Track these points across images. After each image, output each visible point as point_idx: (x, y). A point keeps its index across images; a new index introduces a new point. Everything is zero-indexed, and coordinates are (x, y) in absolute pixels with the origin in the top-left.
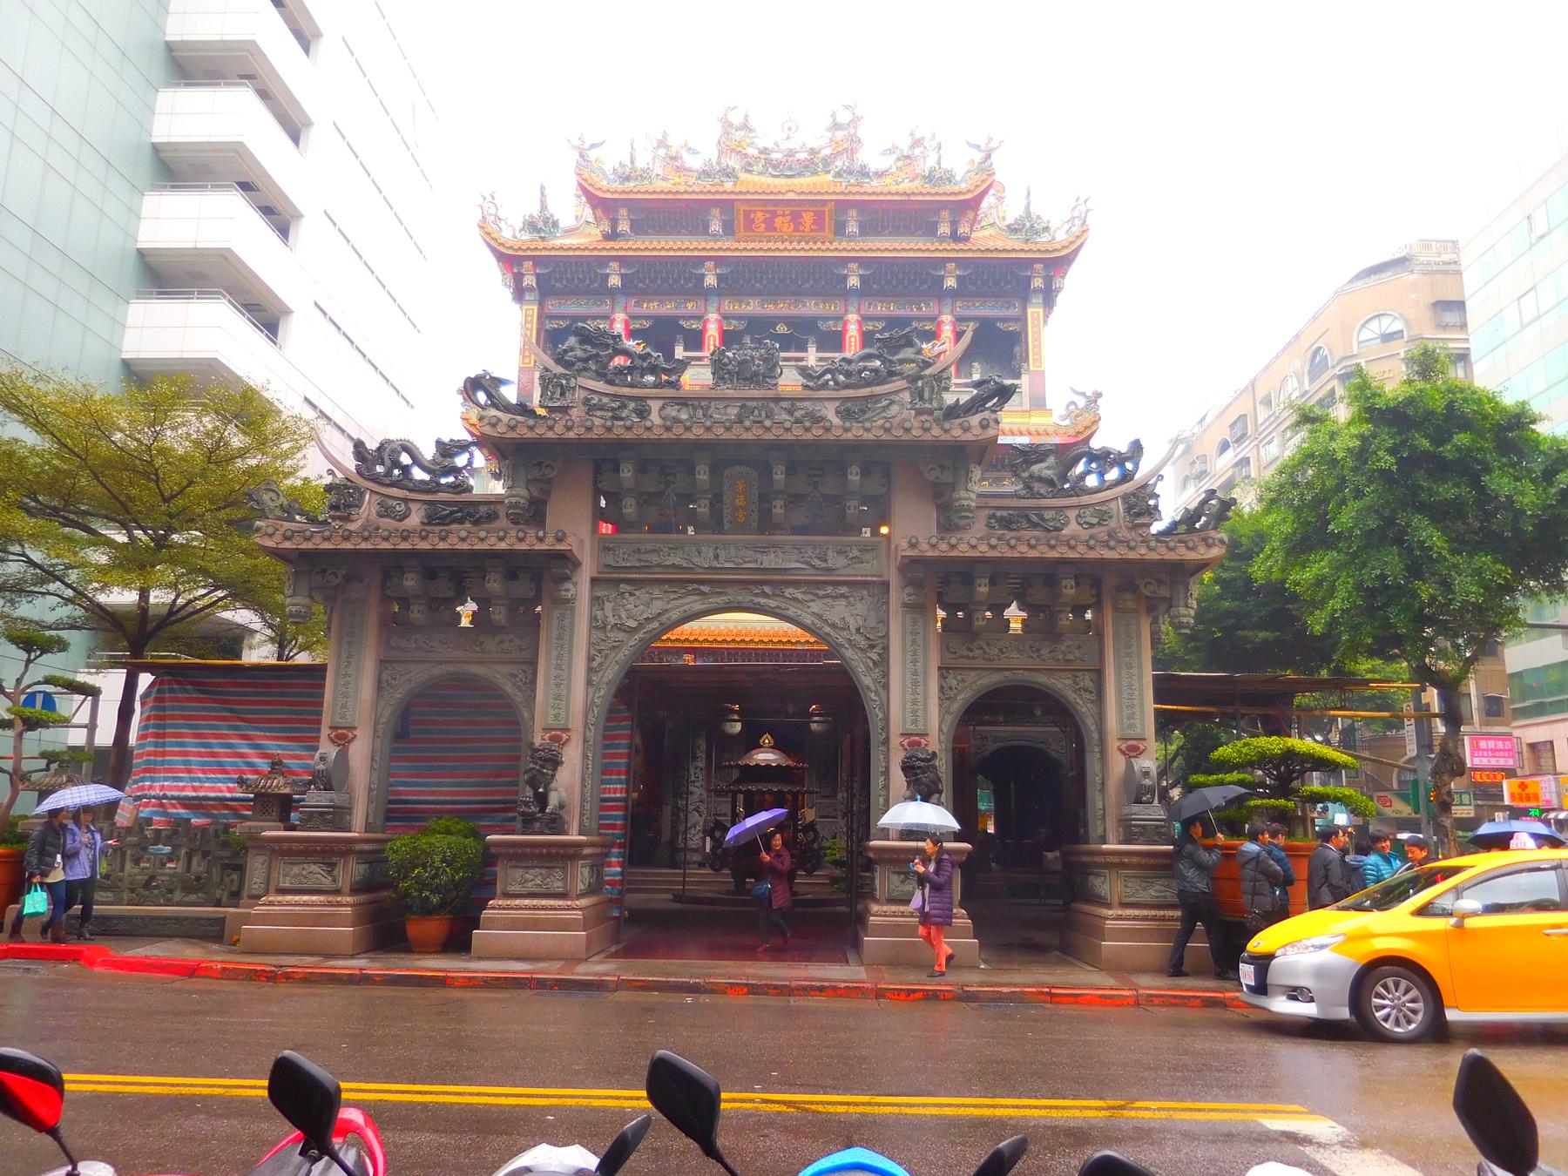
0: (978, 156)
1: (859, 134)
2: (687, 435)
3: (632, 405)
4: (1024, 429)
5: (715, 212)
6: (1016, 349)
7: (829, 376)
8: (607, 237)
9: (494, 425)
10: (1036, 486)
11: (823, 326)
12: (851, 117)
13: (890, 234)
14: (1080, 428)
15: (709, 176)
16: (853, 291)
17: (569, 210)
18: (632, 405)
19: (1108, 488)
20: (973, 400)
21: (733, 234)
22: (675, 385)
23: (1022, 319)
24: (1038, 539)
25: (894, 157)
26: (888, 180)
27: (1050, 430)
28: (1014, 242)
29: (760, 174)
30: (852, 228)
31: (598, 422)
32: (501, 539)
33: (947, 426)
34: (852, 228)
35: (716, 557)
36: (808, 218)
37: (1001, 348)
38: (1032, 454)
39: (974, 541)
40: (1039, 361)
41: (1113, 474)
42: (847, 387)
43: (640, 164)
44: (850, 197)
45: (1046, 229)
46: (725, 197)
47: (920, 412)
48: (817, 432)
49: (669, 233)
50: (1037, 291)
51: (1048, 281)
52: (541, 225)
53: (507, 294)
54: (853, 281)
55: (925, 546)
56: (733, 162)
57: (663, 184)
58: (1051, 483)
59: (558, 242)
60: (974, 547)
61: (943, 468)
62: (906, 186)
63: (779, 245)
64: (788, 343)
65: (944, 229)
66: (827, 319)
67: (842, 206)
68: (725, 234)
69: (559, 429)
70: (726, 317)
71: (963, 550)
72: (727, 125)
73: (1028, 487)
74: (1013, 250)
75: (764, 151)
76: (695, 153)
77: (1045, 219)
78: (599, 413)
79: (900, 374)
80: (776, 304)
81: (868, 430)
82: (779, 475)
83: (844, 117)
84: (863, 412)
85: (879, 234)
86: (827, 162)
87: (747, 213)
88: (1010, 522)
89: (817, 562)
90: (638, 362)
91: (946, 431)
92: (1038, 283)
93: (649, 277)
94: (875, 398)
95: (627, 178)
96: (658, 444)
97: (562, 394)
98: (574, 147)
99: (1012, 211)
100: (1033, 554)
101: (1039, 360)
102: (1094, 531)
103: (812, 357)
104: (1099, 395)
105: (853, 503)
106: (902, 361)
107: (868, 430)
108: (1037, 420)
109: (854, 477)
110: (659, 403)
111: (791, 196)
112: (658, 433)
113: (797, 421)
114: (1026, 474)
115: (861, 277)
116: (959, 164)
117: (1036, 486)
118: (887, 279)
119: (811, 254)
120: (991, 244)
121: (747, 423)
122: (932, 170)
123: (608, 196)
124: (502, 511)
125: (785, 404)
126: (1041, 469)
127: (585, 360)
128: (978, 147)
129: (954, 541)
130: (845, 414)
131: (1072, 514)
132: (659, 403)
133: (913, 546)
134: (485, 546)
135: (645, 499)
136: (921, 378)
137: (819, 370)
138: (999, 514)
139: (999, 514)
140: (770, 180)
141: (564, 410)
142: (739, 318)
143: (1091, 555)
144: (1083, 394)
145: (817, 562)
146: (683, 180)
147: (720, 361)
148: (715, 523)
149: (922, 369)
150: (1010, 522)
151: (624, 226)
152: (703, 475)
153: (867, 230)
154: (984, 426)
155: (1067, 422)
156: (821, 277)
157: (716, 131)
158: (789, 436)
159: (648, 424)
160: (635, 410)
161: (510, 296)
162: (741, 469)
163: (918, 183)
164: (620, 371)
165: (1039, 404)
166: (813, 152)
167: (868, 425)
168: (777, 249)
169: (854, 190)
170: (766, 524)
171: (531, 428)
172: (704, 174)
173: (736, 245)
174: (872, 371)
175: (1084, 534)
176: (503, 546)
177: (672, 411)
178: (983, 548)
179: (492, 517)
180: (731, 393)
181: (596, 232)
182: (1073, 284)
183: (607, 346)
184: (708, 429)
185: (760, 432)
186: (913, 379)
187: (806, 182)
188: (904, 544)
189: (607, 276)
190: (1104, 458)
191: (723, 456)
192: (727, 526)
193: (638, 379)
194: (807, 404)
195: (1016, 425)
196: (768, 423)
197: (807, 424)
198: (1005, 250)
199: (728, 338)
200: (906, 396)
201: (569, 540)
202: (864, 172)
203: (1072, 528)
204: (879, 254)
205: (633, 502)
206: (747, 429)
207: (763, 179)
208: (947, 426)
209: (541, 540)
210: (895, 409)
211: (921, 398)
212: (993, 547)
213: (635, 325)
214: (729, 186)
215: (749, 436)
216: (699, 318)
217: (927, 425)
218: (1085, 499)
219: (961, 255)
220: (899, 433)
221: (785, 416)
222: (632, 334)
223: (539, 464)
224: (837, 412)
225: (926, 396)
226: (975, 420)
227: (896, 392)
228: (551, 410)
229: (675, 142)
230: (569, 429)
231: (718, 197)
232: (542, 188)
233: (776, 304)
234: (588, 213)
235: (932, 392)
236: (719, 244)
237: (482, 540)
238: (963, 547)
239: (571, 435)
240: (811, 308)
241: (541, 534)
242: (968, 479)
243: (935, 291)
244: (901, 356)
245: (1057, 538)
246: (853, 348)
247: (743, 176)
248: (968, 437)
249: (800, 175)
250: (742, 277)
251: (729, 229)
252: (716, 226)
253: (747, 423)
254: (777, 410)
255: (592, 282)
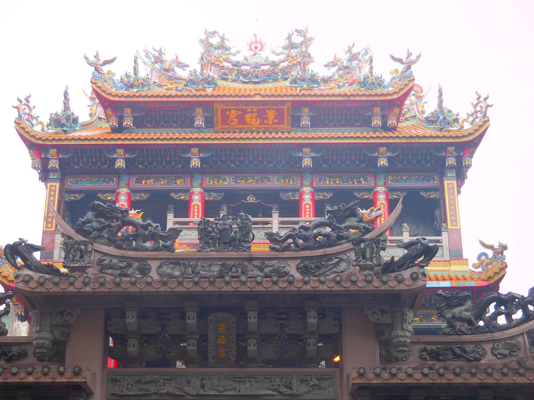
0: (400, 67)
1: (310, 50)
2: (180, 289)
3: (136, 265)
4: (446, 275)
5: (199, 110)
6: (437, 212)
7: (290, 240)
8: (114, 130)
9: (27, 282)
10: (458, 324)
11: (284, 197)
12: (302, 39)
13: (335, 126)
14: (491, 273)
15: (194, 83)
16: (307, 170)
17: (84, 109)
18: (136, 265)
19: (515, 326)
20: (404, 258)
21: (213, 127)
22: (170, 249)
23: (440, 189)
24: (461, 368)
25: (337, 67)
26: (332, 85)
27: (467, 275)
28: (431, 131)
29: (233, 81)
30: (305, 121)
31: (109, 278)
32: (30, 374)
33: (385, 278)
34: (305, 121)
35: (203, 386)
36: (271, 114)
37: (427, 212)
38: (453, 297)
39: (410, 371)
40: (456, 221)
41: (518, 315)
42: (305, 248)
43: (143, 73)
44: (304, 99)
45: (456, 120)
46: (207, 99)
47: (363, 268)
48: (283, 285)
49: (163, 127)
50: (451, 167)
51: (459, 159)
52: (64, 121)
53: (36, 174)
54: (307, 162)
55: (370, 375)
56: (213, 73)
57: (160, 90)
58: (470, 322)
59: (77, 134)
60: (410, 376)
61: (382, 311)
62: (346, 89)
63: (248, 135)
64: (254, 210)
65: (377, 122)
66: (287, 191)
67: (297, 105)
68: (207, 127)
69: (78, 284)
70: (207, 190)
71: (402, 378)
72: (208, 46)
73: (451, 325)
74: (431, 137)
75: (237, 64)
76: (184, 66)
77: (455, 112)
78: (110, 271)
79: (347, 238)
80: (247, 180)
81: (322, 283)
82: (253, 319)
83: (297, 39)
84: (318, 268)
85: (326, 126)
86: (285, 72)
87: (281, 122)
88: (438, 354)
89: (284, 390)
90: (141, 231)
91: (385, 283)
92: (451, 161)
93: (146, 160)
94: (328, 257)
95: (131, 86)
96: (156, 296)
97: (82, 257)
98: (90, 64)
99: (430, 107)
100: (458, 380)
101: (456, 221)
102: (507, 360)
103: (275, 223)
104: (505, 248)
105: (312, 341)
106: (348, 228)
107: (322, 283)
108: (456, 268)
109: (312, 320)
110: (158, 263)
111: (258, 98)
112: (157, 287)
113: (266, 276)
114: (449, 315)
115: (313, 159)
116: (385, 71)
117: (458, 324)
118: (330, 159)
119: (274, 141)
120: (414, 132)
121: (227, 279)
122: (366, 78)
123: (117, 99)
124: (30, 350)
125: (256, 263)
126: (464, 311)
127: (100, 230)
128: (400, 61)
129: (394, 371)
130: (304, 270)
131: (488, 347)
132: (158, 263)
133: (361, 375)
134: (16, 380)
135: (146, 339)
136: (364, 241)
137: (283, 233)
138: (429, 348)
139: (429, 348)
140: (241, 86)
141: (82, 269)
142: (217, 191)
143: (505, 381)
144: (491, 247)
145: (284, 390)
146: (174, 86)
147: (205, 229)
148: (201, 359)
149: (364, 234)
150: (438, 354)
151: (128, 122)
152: (192, 321)
153: (316, 123)
154: (414, 278)
155: (480, 270)
156: (284, 160)
157: (200, 50)
158: (260, 288)
159: (149, 280)
160: (138, 269)
161: (37, 176)
162: (221, 315)
163: (355, 86)
164: (126, 239)
165: (457, 255)
166: (274, 64)
167: (322, 279)
168: (248, 138)
169: (306, 93)
170: (242, 358)
171: (56, 284)
172: (190, 82)
173: (216, 135)
174: (325, 235)
175: (499, 363)
176: (31, 379)
177: (167, 270)
178: (418, 376)
179: (22, 355)
180: (215, 254)
181: (106, 126)
182: (480, 161)
183: (117, 219)
184: (196, 283)
185: (238, 285)
186: (357, 242)
187: (268, 87)
188: (354, 374)
189: (115, 159)
190: (510, 302)
191: (209, 305)
192: (211, 361)
193: (141, 244)
194: (274, 262)
195: (439, 274)
196: (243, 278)
197: (275, 279)
198: (425, 137)
199: (209, 208)
200: (352, 256)
201: (85, 374)
202: (313, 79)
203: (489, 358)
204: (326, 141)
205: (136, 342)
206: (227, 283)
207: (236, 85)
208: (385, 278)
209: (62, 374)
210: (343, 266)
211: (364, 257)
212: (425, 375)
213: (136, 197)
214: (209, 91)
215: (228, 288)
216: (186, 191)
217: (369, 278)
218: (497, 335)
219: (391, 141)
220: (348, 284)
221: (256, 272)
222: (133, 205)
223: (62, 313)
224: (298, 269)
225: (368, 255)
226: (406, 274)
227: (344, 252)
228: (72, 269)
229: (169, 57)
230: (86, 284)
231: (201, 99)
232: (66, 94)
233: (247, 180)
234: (100, 111)
235: (372, 252)
236: (202, 135)
237: (14, 375)
238: (402, 375)
239: (88, 289)
240: (274, 183)
241: (62, 369)
242: (403, 320)
243: (371, 168)
244: (347, 224)
245: (477, 368)
246: (308, 217)
247: (221, 83)
248: (402, 287)
249: (264, 81)
250: (220, 159)
251: (209, 123)
252: (199, 122)
253: (227, 279)
254: (250, 267)
255: (103, 164)
